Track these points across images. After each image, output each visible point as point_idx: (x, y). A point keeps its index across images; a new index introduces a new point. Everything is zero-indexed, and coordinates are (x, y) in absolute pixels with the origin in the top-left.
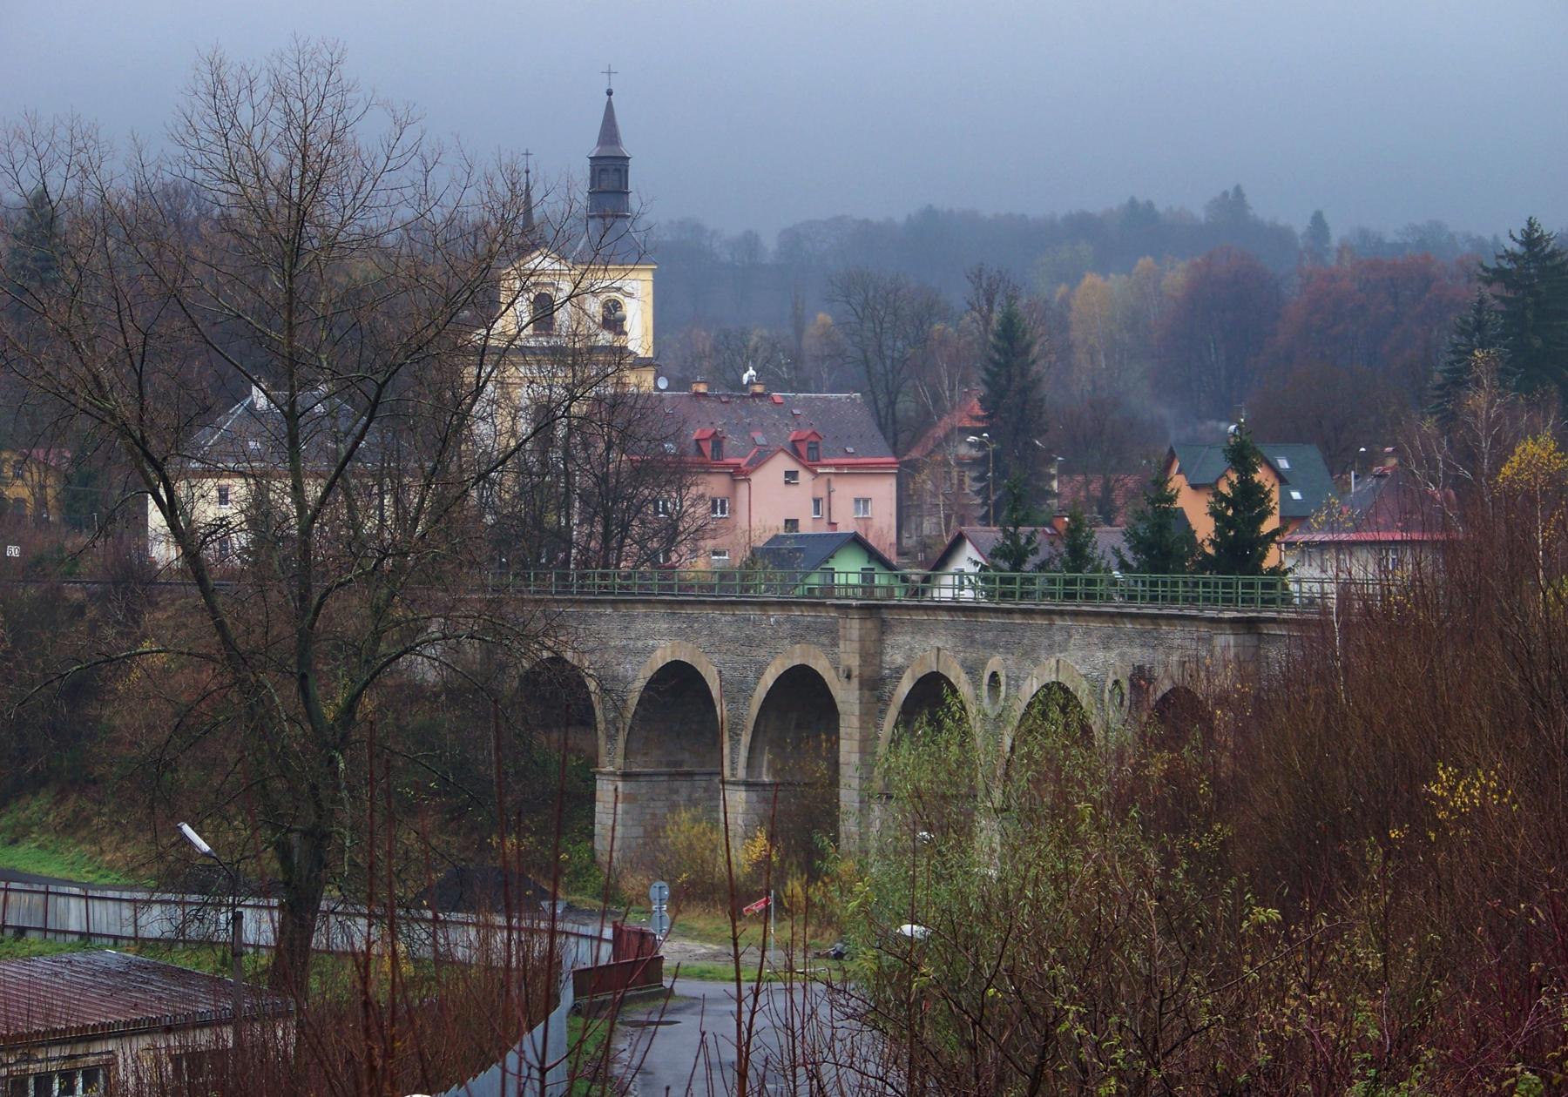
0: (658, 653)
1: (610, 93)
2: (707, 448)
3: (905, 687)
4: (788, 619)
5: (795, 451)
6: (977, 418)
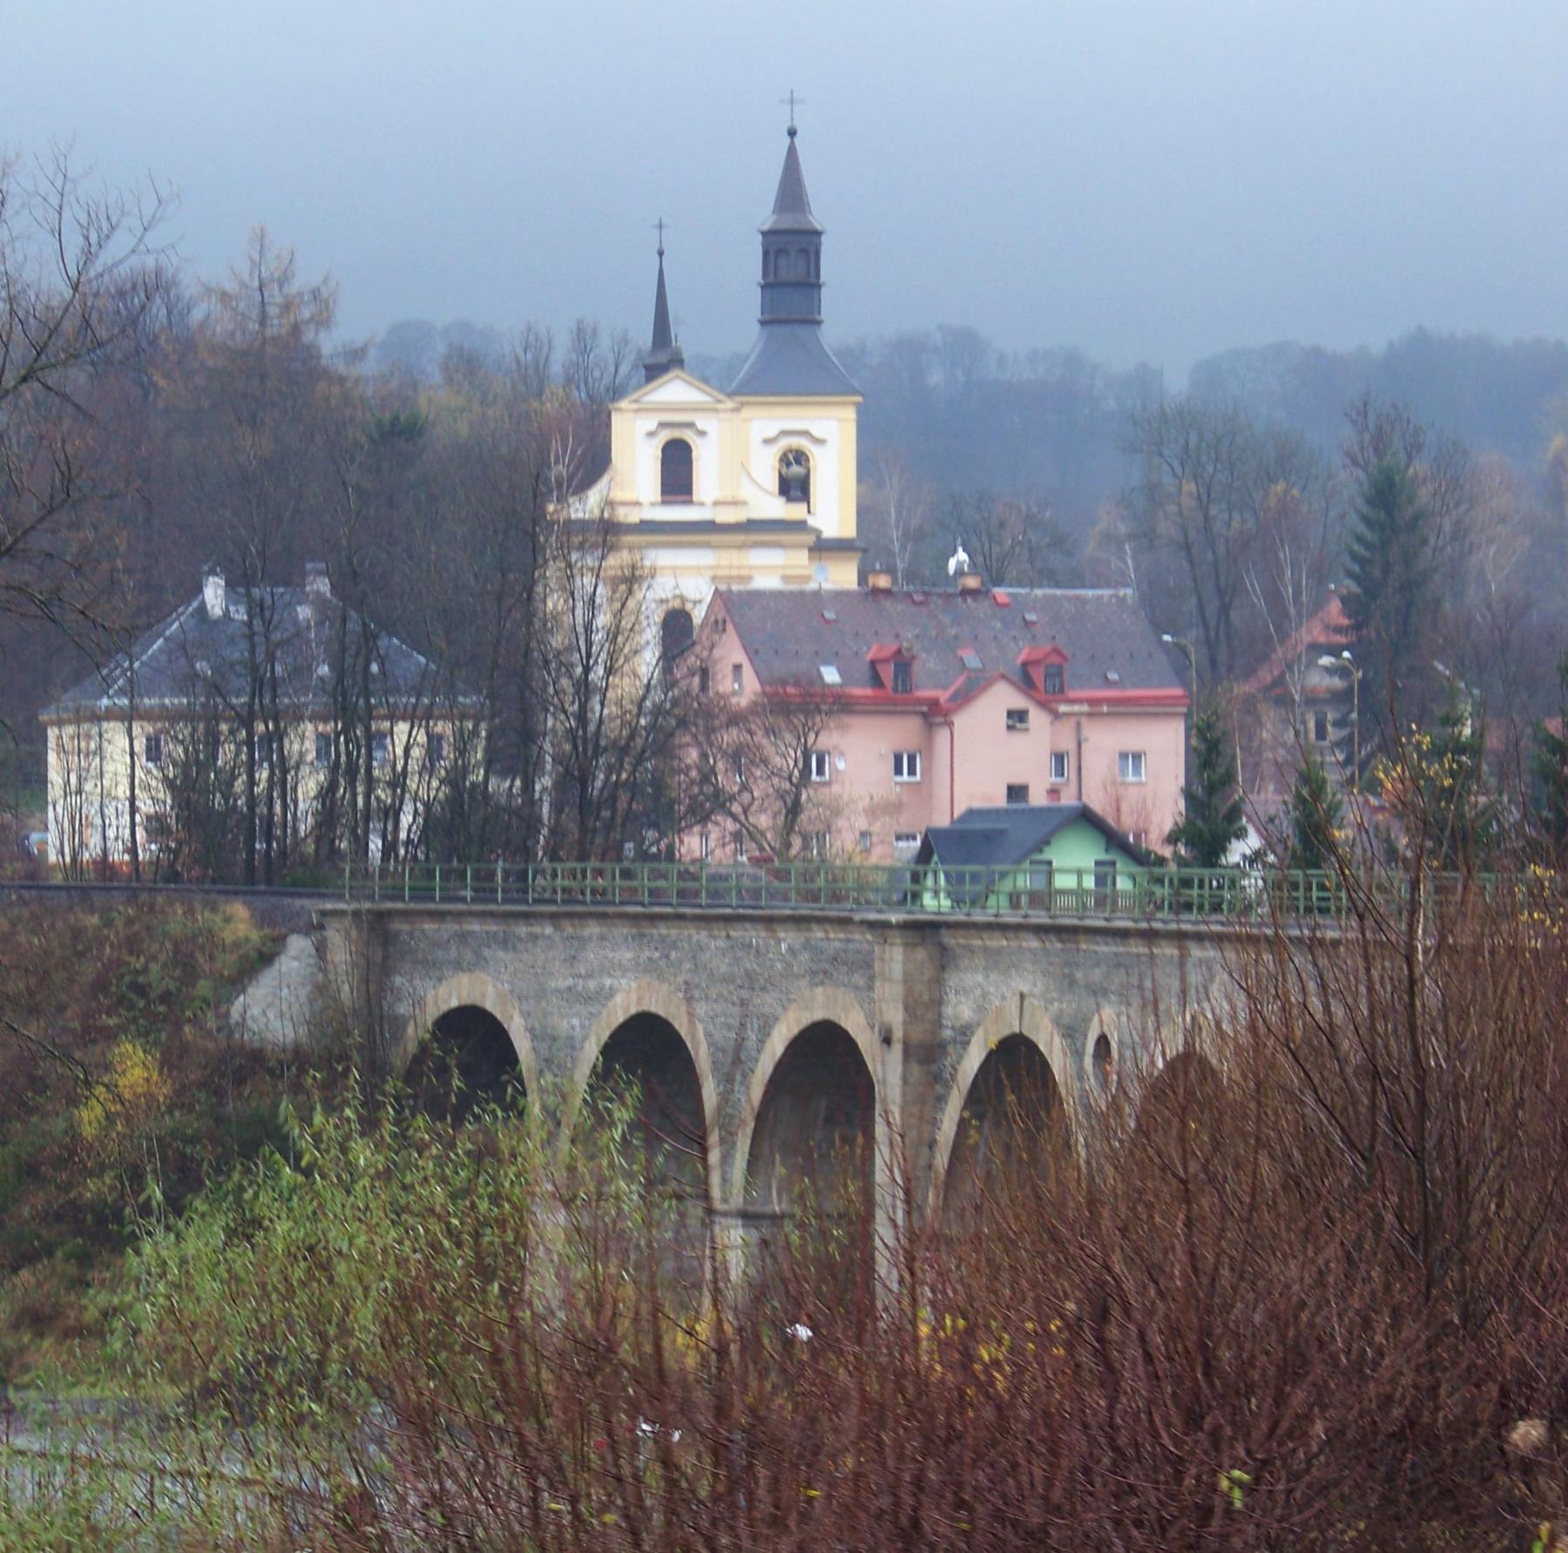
0: (619, 999)
1: (792, 133)
2: (887, 673)
3: (973, 1060)
4: (807, 945)
5: (1025, 681)
6: (1339, 630)
